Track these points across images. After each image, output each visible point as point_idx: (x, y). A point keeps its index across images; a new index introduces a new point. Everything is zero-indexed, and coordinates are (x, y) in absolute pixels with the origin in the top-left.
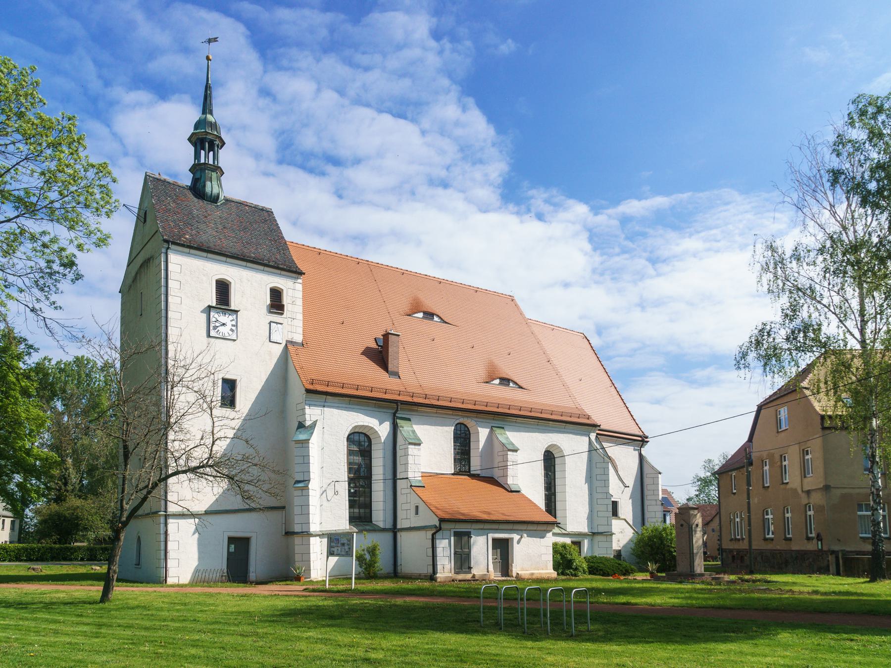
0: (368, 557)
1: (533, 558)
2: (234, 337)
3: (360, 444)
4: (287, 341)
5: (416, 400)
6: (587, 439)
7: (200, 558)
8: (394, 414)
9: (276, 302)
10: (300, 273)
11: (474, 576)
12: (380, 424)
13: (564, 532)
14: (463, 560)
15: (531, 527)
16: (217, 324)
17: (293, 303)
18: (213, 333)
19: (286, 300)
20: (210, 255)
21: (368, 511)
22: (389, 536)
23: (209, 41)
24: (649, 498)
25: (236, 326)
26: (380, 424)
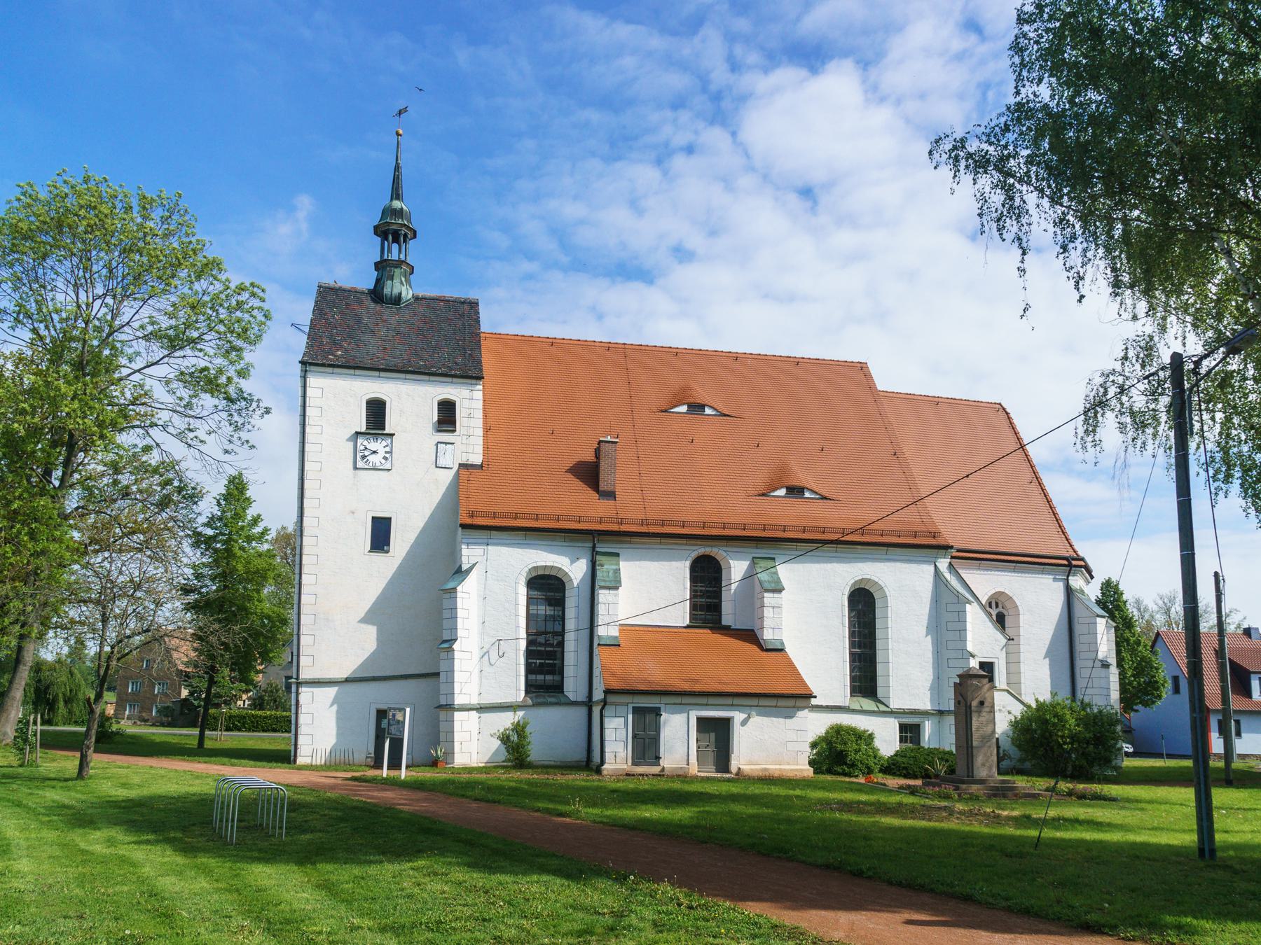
0: (515, 738)
1: (772, 747)
2: (388, 466)
3: (547, 587)
4: (461, 465)
5: (623, 528)
6: (932, 568)
7: (340, 734)
8: (594, 547)
9: (447, 416)
10: (480, 378)
11: (663, 769)
12: (572, 562)
13: (882, 708)
14: (646, 745)
15: (763, 702)
16: (366, 453)
17: (469, 416)
18: (360, 464)
19: (460, 413)
20: (358, 372)
21: (557, 678)
22: (583, 711)
23: (400, 113)
24: (1083, 655)
25: (390, 452)
26: (572, 562)
